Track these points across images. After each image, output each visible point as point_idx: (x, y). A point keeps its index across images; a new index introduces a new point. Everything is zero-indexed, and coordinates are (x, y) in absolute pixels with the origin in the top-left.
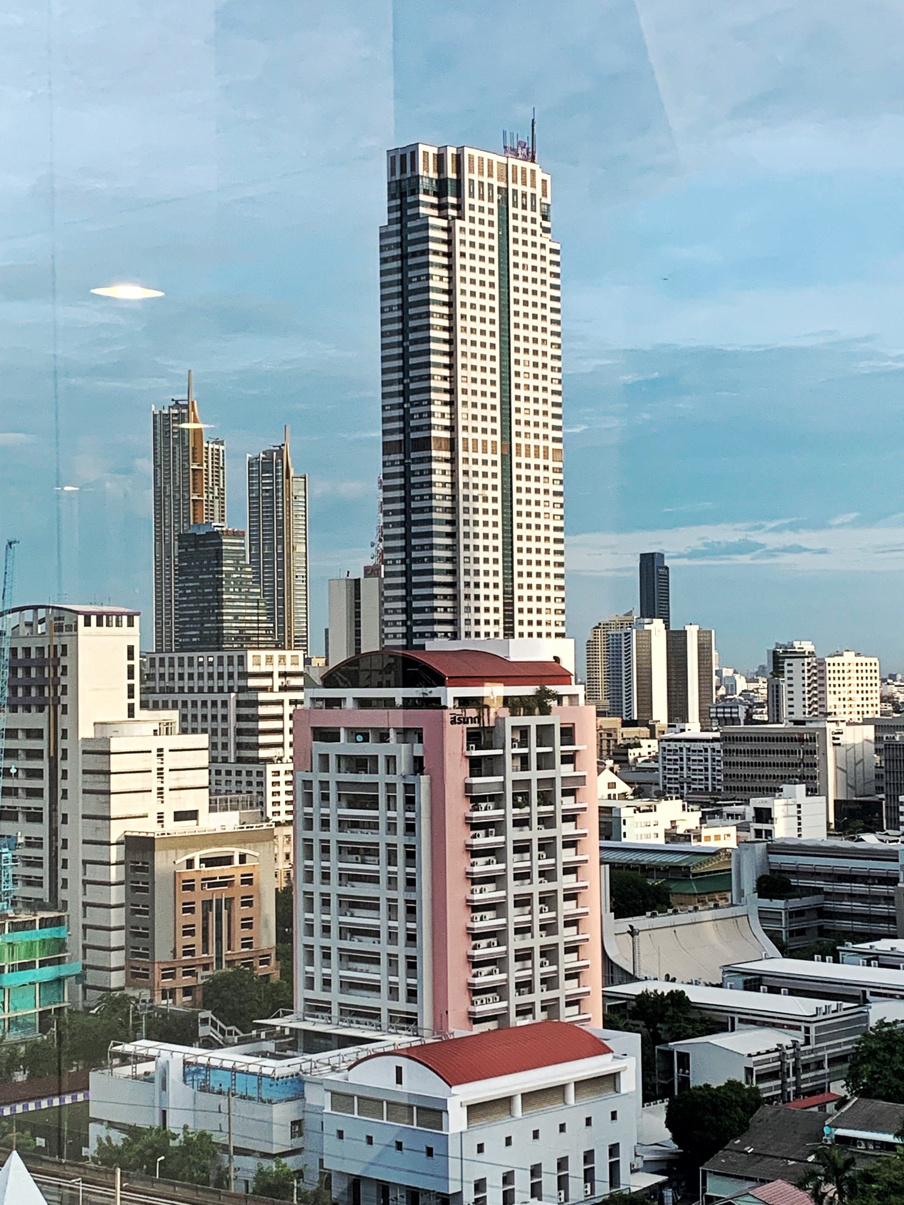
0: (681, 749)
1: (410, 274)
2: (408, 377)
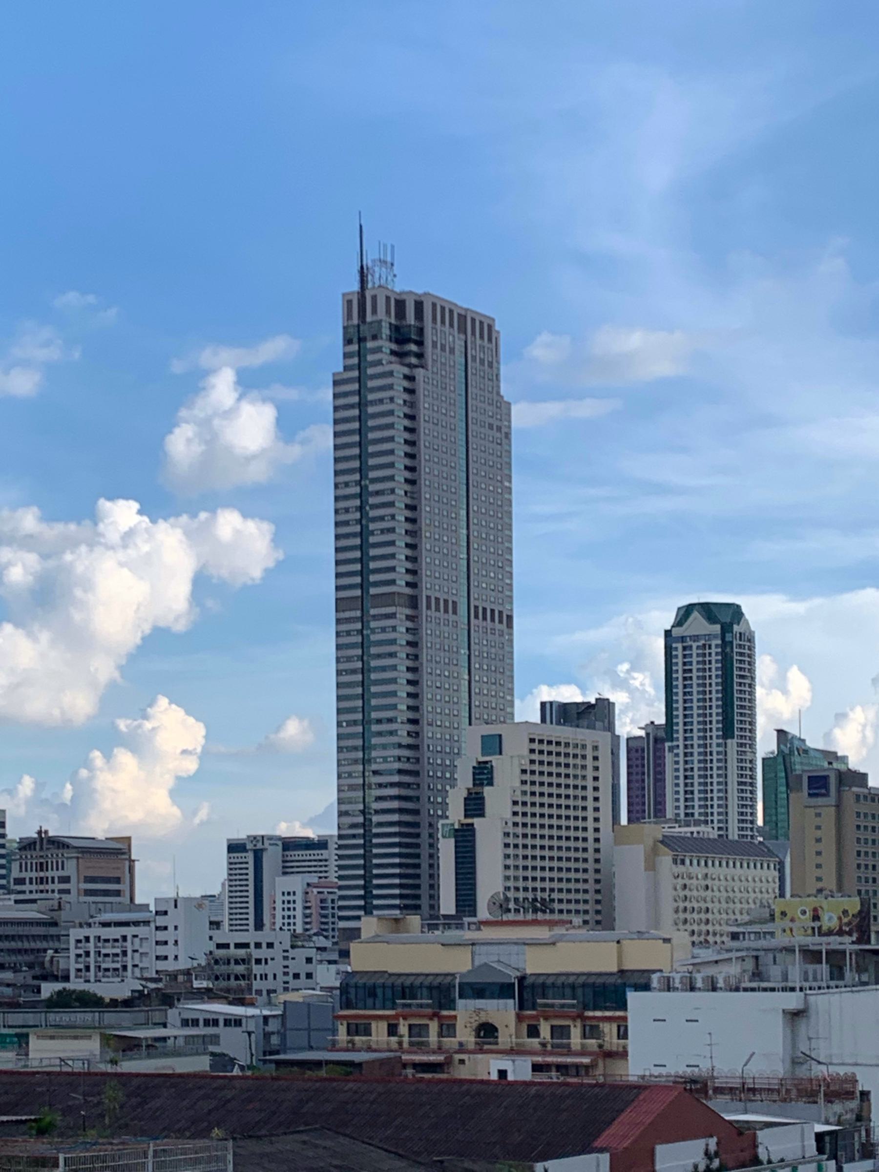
0: (124, 938)
1: (373, 624)
2: (369, 628)
